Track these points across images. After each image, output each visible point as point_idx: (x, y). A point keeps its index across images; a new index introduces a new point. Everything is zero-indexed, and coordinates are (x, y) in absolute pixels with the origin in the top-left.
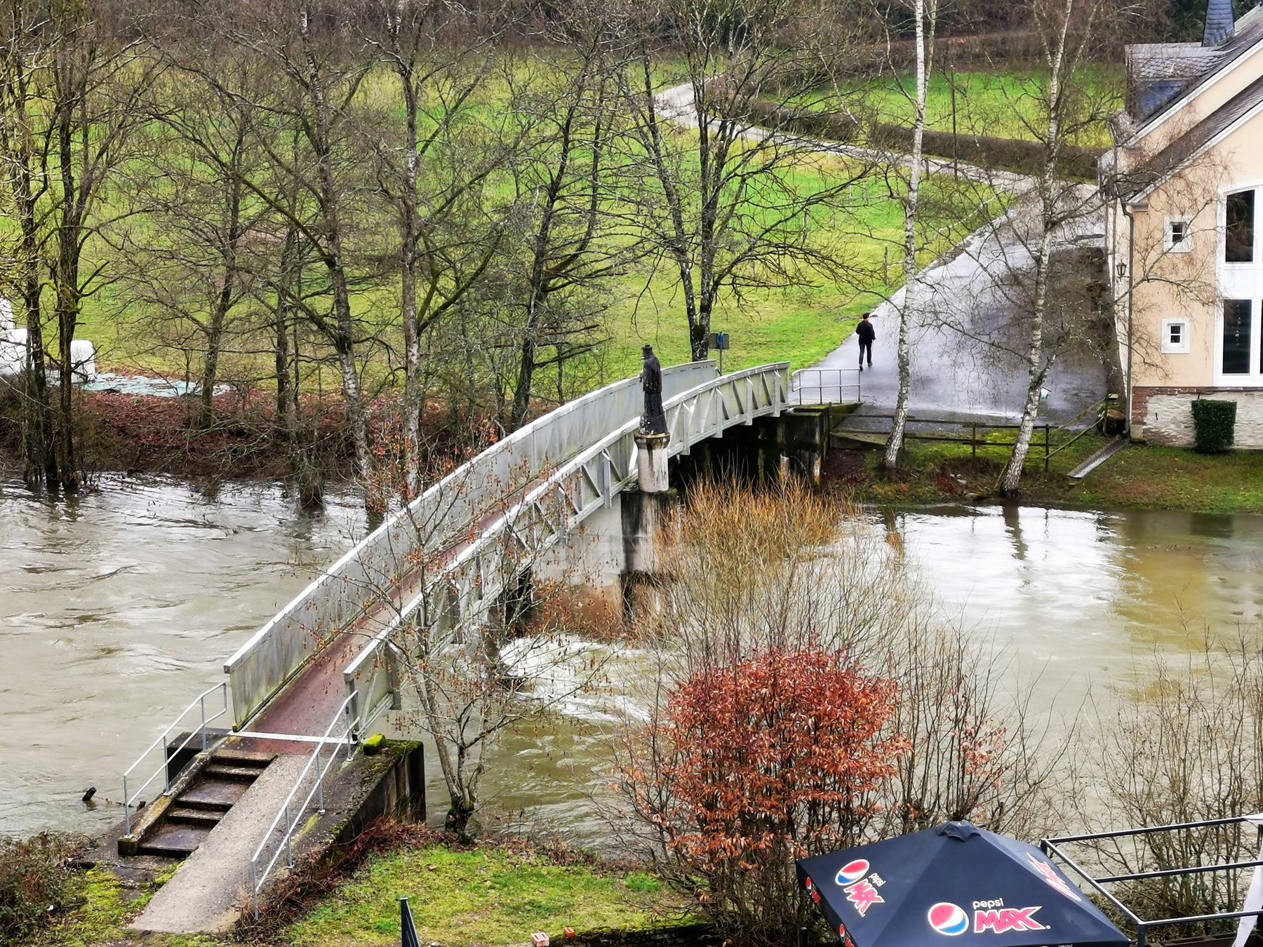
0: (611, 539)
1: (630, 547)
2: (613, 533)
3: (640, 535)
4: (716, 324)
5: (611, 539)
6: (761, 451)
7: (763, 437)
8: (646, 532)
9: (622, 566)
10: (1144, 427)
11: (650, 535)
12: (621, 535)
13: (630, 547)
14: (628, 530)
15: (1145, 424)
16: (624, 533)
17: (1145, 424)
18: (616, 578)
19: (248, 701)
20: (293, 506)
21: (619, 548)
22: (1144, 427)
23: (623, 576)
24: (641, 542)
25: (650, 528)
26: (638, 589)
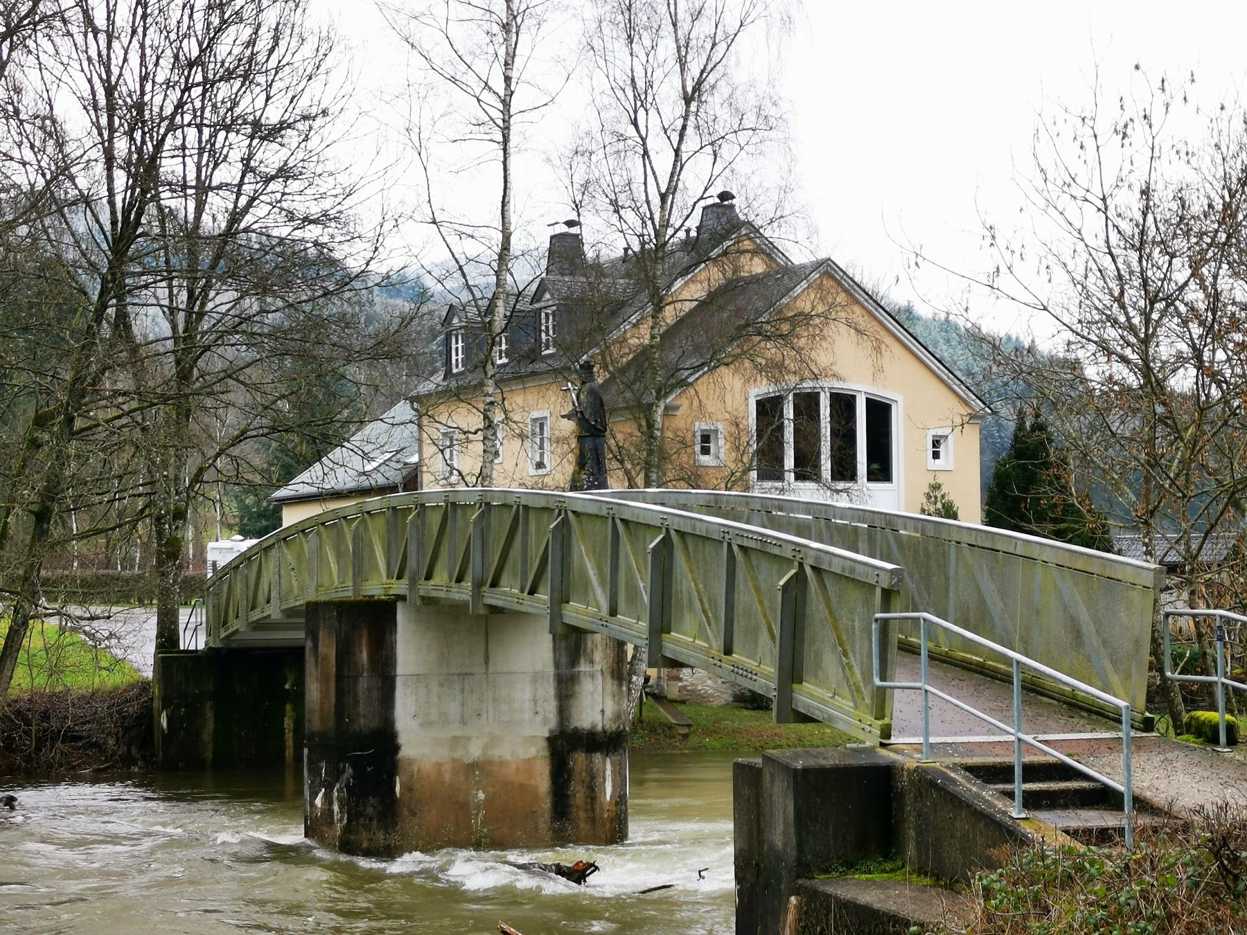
0: (536, 678)
1: (566, 686)
2: (539, 667)
3: (583, 667)
4: (230, 408)
5: (536, 678)
6: (288, 707)
7: (292, 686)
8: (592, 662)
9: (553, 722)
10: (680, 684)
11: (598, 667)
12: (550, 670)
13: (566, 686)
14: (564, 660)
15: (681, 680)
16: (557, 665)
17: (681, 680)
18: (544, 744)
19: (335, 845)
20: (1162, 802)
21: (548, 691)
22: (680, 684)
23: (552, 741)
24: (582, 678)
25: (598, 656)
26: (579, 760)
